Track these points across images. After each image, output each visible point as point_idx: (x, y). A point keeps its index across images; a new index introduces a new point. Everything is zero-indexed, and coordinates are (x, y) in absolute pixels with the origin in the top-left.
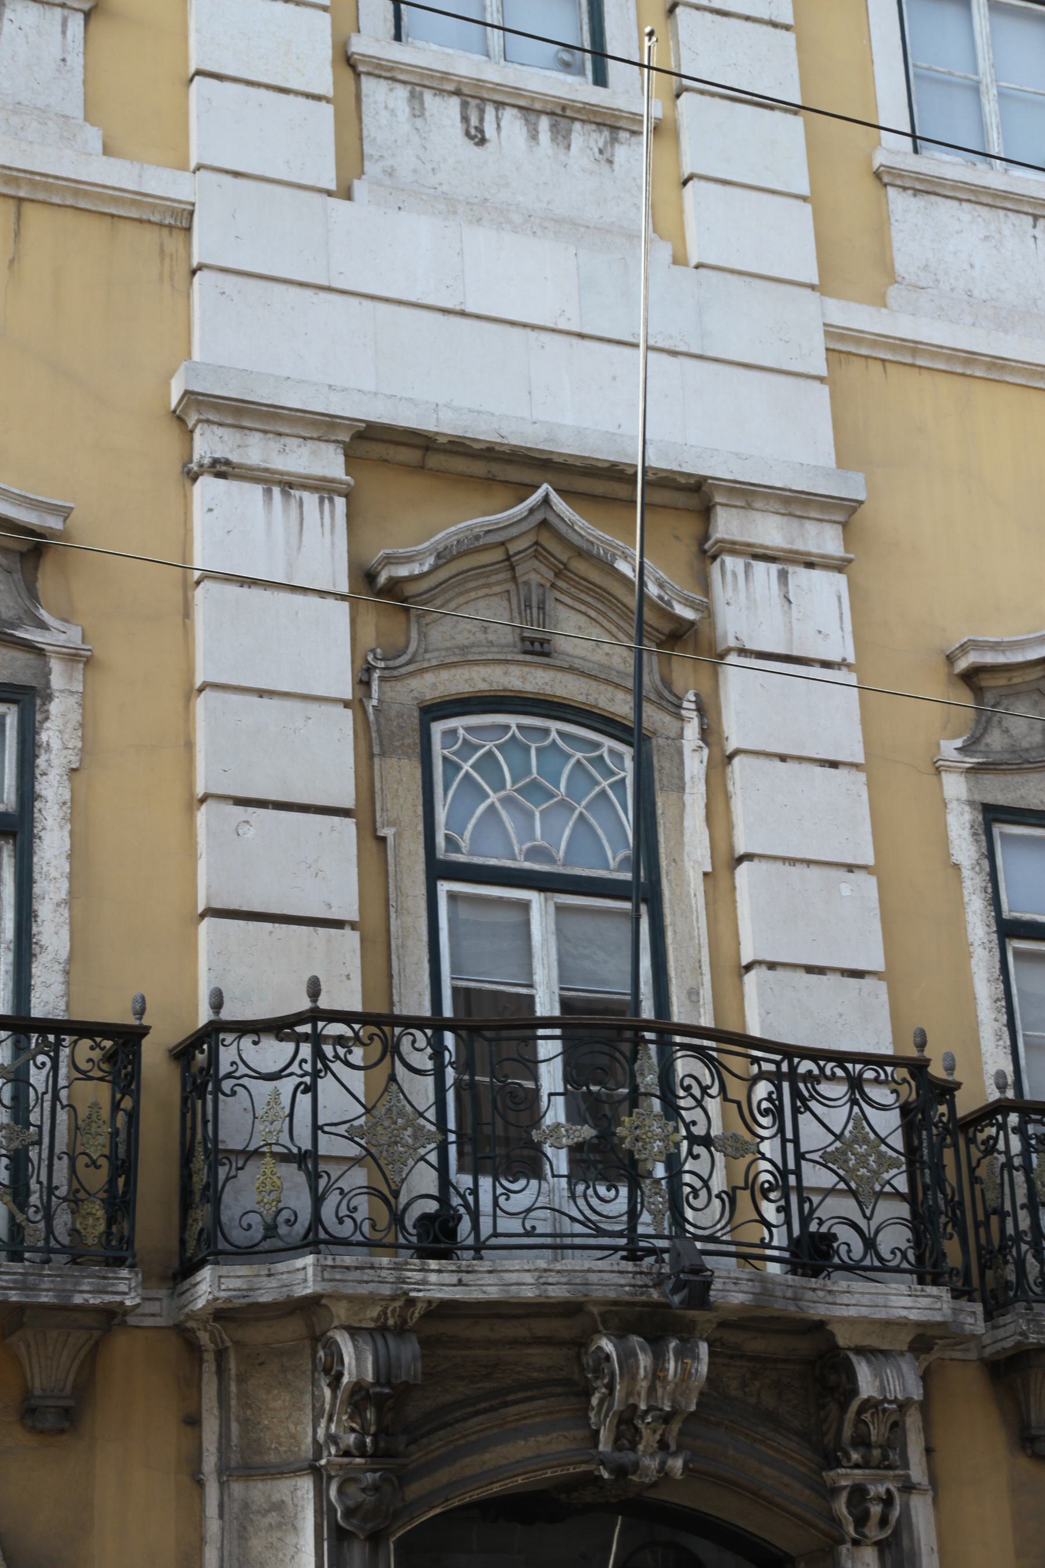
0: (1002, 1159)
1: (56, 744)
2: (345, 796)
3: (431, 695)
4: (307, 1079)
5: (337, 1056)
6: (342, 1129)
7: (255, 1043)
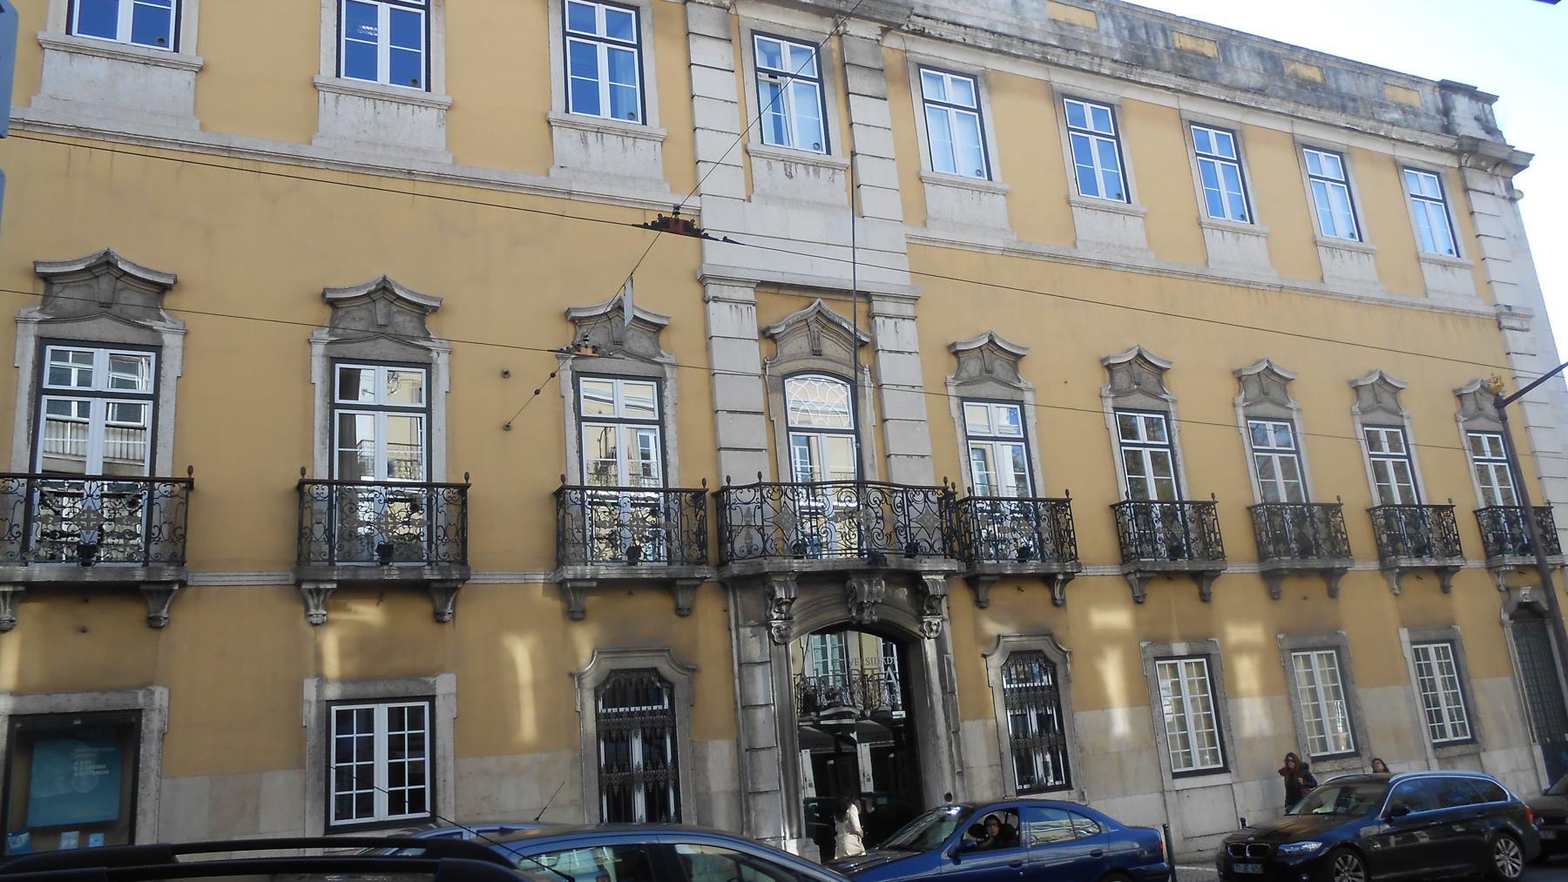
0: (970, 515)
1: (670, 396)
2: (761, 407)
3: (785, 372)
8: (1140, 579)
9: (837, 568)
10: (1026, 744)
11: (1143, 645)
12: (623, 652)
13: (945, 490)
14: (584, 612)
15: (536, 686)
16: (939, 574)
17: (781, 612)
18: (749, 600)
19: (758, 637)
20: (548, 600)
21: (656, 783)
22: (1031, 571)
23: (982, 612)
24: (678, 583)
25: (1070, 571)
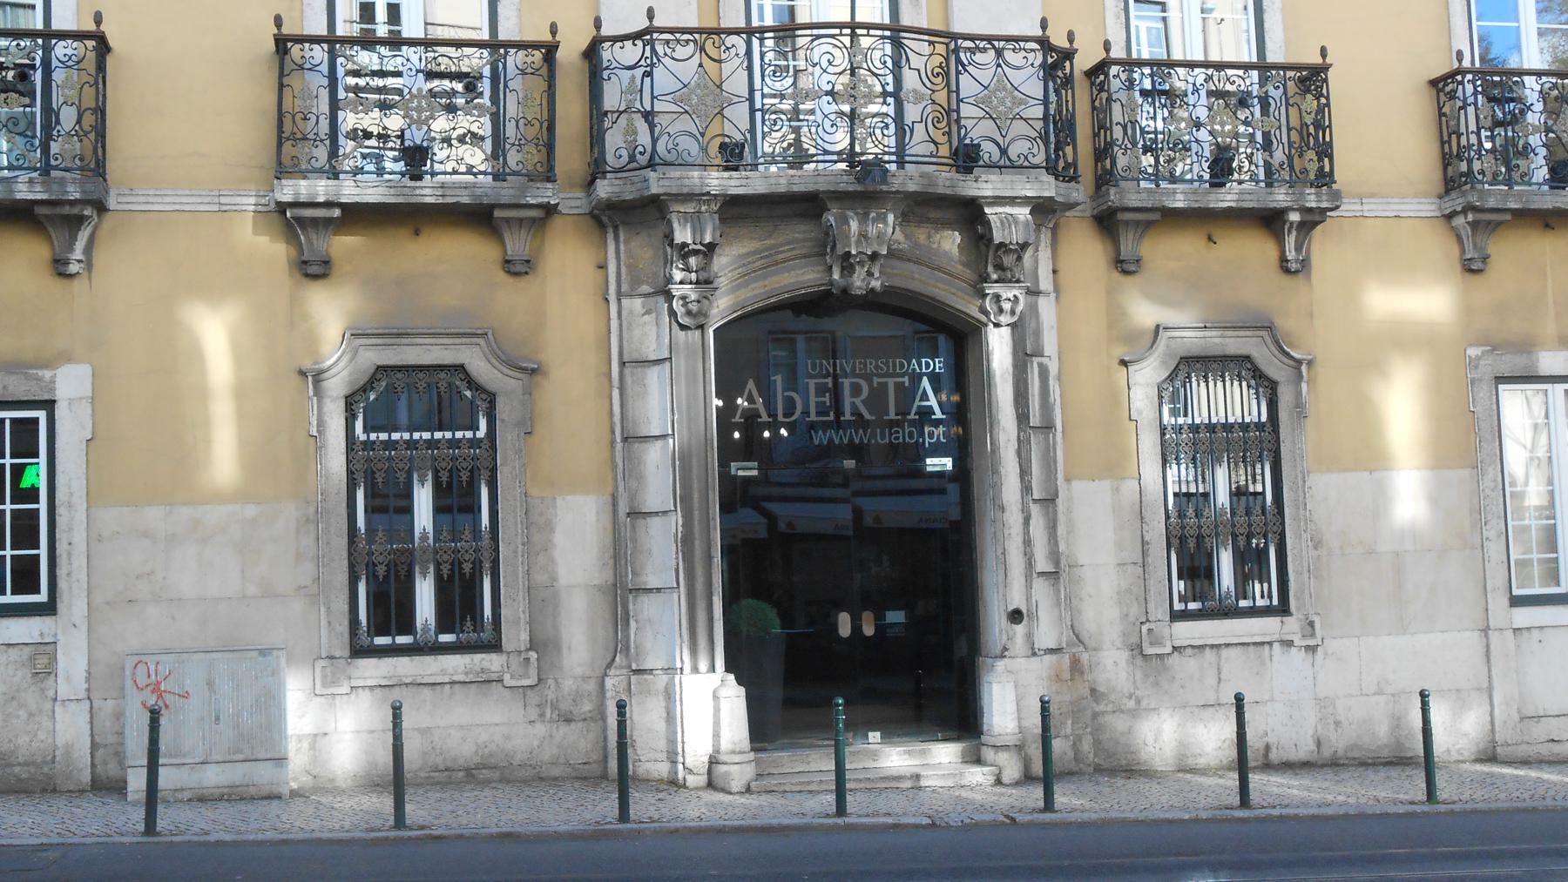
4: (648, 69)
5: (666, 54)
6: (668, 98)
7: (622, 48)
8: (1474, 225)
9: (795, 188)
10: (1250, 525)
11: (1473, 352)
12: (399, 335)
13: (1045, 44)
14: (326, 263)
15: (241, 393)
16: (1020, 205)
17: (688, 269)
18: (640, 247)
19: (654, 315)
20: (264, 241)
21: (456, 565)
22: (1226, 205)
23: (1128, 280)
24: (1122, 216)
25: (1313, 205)
